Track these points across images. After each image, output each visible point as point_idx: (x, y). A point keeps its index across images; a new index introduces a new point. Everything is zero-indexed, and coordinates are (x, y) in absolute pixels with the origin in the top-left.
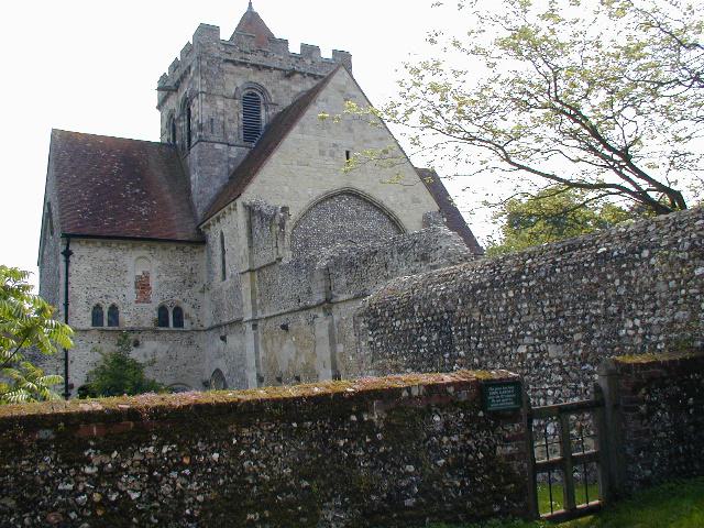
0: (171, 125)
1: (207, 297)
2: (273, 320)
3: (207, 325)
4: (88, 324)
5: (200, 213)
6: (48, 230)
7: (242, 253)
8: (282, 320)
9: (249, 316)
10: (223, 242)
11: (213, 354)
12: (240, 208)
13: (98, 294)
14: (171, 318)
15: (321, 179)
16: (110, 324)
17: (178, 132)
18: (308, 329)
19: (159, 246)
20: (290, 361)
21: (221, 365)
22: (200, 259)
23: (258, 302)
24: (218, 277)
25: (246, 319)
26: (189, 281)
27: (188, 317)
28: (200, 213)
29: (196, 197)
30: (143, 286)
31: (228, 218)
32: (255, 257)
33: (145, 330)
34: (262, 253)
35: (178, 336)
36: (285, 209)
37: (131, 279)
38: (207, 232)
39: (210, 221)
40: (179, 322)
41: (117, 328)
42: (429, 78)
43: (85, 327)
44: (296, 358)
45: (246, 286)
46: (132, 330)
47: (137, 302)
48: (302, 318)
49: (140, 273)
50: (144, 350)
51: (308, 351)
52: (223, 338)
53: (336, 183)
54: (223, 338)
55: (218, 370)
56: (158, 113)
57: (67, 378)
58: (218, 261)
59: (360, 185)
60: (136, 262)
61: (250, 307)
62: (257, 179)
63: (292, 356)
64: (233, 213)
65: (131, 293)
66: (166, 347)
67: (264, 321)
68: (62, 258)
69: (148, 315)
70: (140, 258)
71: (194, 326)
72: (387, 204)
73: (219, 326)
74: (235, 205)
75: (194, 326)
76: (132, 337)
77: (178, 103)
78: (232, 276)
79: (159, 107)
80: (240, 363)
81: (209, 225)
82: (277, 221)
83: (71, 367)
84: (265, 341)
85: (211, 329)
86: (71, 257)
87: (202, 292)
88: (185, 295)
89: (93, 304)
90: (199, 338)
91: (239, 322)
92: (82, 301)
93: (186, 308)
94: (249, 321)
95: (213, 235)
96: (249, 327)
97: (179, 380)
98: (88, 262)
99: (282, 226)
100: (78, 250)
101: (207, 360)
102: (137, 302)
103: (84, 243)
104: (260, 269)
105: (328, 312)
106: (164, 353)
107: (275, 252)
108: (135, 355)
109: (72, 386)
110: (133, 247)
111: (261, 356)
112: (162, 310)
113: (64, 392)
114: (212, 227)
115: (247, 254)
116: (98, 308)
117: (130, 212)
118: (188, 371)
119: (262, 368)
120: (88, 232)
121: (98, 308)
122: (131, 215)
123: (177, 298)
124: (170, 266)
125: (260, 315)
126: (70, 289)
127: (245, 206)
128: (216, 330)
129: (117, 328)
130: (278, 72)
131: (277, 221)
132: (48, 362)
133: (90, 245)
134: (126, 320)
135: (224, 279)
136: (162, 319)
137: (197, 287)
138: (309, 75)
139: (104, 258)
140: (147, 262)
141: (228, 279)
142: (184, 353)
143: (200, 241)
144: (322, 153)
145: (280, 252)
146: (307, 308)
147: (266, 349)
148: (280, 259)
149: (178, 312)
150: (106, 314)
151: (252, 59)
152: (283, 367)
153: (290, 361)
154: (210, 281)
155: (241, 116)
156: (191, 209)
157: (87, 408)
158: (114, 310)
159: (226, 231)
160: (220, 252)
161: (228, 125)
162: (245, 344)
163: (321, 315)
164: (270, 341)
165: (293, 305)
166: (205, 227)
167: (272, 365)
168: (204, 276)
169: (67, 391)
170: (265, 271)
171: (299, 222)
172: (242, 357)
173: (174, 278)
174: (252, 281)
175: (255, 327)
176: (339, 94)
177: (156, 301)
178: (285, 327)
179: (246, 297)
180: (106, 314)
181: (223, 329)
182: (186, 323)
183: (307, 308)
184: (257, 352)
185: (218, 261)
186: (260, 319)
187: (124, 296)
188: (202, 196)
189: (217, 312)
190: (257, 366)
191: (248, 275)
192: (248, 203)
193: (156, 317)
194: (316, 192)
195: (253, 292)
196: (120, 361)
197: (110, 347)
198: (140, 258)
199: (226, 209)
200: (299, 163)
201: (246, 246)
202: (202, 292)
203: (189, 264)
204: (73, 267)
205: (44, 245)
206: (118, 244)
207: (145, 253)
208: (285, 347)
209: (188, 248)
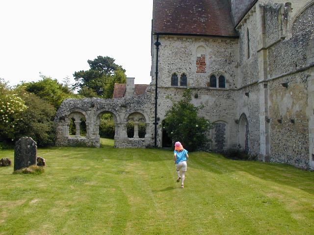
1: (239, 70)
2: (278, 81)
3: (239, 87)
4: (169, 84)
5: (236, 20)
7: (258, 38)
8: (284, 80)
9: (262, 79)
10: (248, 35)
11: (241, 104)
12: (258, 9)
13: (175, 67)
14: (217, 82)
16: (182, 84)
18: (302, 85)
19: (211, 40)
20: (288, 109)
21: (245, 110)
22: (236, 47)
23: (268, 69)
24: (245, 58)
25: (260, 81)
26: (229, 60)
27: (228, 82)
28: (236, 20)
29: (233, 12)
30: (201, 63)
31: (251, 18)
32: (267, 39)
33: (201, 88)
34: (272, 36)
35: (221, 93)
36: (288, 4)
37: (194, 59)
38: (240, 30)
40: (222, 85)
41: (185, 87)
43: (167, 86)
44: (292, 106)
45: (261, 59)
46: (194, 89)
47: (197, 72)
48: (298, 78)
49: (199, 55)
50: (201, 100)
51: (301, 102)
52: (247, 94)
54: (247, 94)
55: (244, 114)
57: (156, 114)
58: (245, 47)
60: (197, 49)
61: (263, 72)
63: (290, 106)
64: (254, 14)
65: (194, 67)
66: (214, 99)
67: (271, 82)
69: (204, 80)
70: (199, 46)
71: (231, 87)
73: (245, 87)
75: (231, 87)
76: (194, 92)
78: (253, 54)
80: (256, 110)
81: (241, 26)
82: (282, 11)
83: (158, 108)
84: (271, 95)
85: (240, 89)
86: (160, 47)
87: (237, 67)
88: (226, 69)
89: (172, 73)
90: (234, 95)
91: (256, 83)
92: (165, 71)
93: (227, 76)
95: (243, 32)
96: (262, 86)
97: (221, 119)
98: (169, 46)
99: (286, 15)
100: (163, 42)
101: (238, 108)
102: (197, 72)
103: (166, 38)
104: (269, 48)
106: (213, 103)
107: (280, 33)
108: (195, 103)
109: (159, 119)
110: (196, 40)
111: (269, 106)
112: (213, 77)
113: (154, 122)
114: (242, 27)
115: (262, 37)
116: (175, 75)
117: (195, 21)
118: (227, 114)
119: (269, 113)
120: (169, 31)
121: (175, 75)
122: (195, 22)
123: (221, 70)
125: (269, 78)
126: (159, 64)
127: (260, 6)
129: (185, 87)
131: (282, 11)
132: (146, 105)
134: (191, 82)
135: (249, 57)
136: (212, 83)
137: (234, 64)
139: (178, 47)
140: (204, 49)
142: (224, 103)
143: (236, 37)
145: (284, 33)
146: (302, 70)
147: (272, 101)
148: (283, 38)
149: (222, 79)
150: (179, 80)
152: (283, 113)
153: (288, 109)
154: (241, 59)
156: (231, 17)
157: (13, 165)
158: (184, 76)
159: (250, 27)
160: (247, 41)
162: (259, 97)
164: (275, 95)
165: (291, 69)
166: (238, 28)
167: (276, 112)
168: (237, 58)
170: (273, 48)
171: (298, 17)
172: (257, 107)
174: (265, 55)
175: (265, 86)
177: (209, 72)
178: (285, 85)
179: (261, 66)
180: (179, 80)
181: (247, 89)
182: (227, 85)
183: (302, 70)
184: (266, 103)
185: (245, 47)
186: (269, 81)
187: (191, 69)
188: (237, 10)
189: (245, 79)
190: (266, 111)
192: (263, 4)
193: (209, 81)
195: (265, 63)
196: (184, 106)
197: (179, 98)
201: (261, 33)
202: (237, 67)
203: (230, 50)
204: (161, 52)
206: (187, 39)
207: (202, 44)
208: (285, 99)
209: (228, 41)
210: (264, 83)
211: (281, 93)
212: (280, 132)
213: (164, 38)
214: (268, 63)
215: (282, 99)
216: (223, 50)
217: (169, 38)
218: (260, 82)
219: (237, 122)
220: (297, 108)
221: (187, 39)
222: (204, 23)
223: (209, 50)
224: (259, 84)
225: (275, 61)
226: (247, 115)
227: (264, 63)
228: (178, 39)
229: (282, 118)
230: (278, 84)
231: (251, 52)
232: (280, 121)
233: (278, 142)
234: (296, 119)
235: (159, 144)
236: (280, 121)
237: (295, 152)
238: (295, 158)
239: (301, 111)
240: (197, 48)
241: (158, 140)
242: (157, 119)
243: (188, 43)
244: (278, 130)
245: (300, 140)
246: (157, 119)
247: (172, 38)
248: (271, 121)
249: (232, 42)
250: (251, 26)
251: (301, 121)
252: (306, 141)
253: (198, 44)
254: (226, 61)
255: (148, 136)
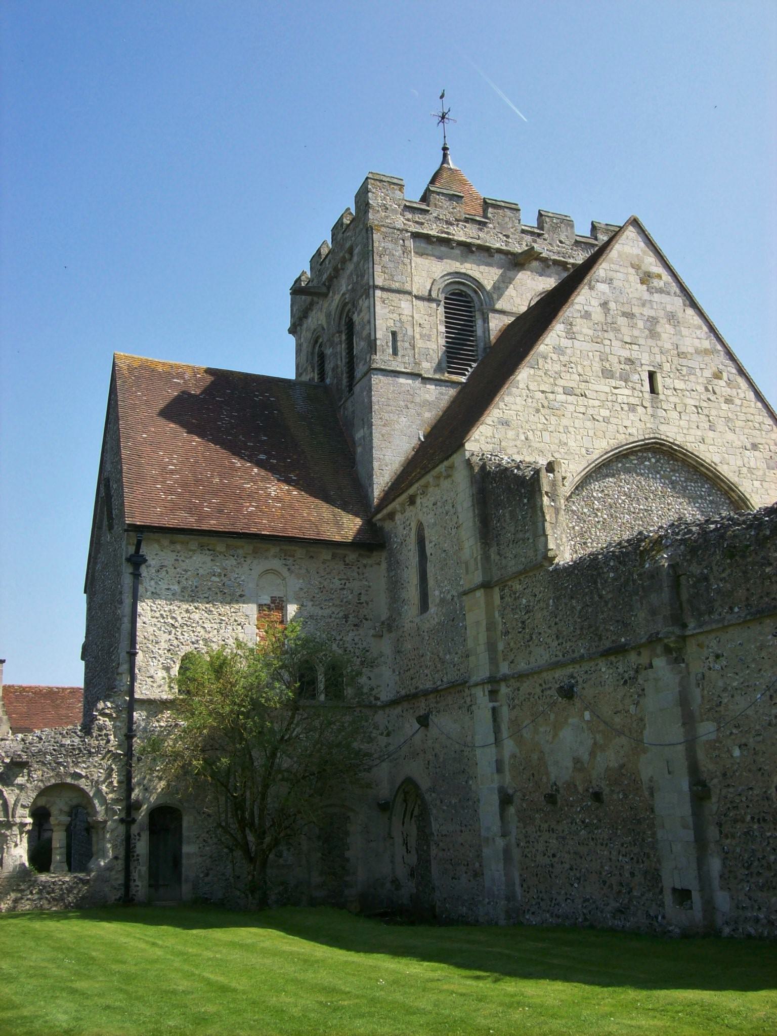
0: (313, 354)
6: (105, 523)
9: (484, 672)
15: (606, 420)
17: (329, 366)
20: (577, 761)
23: (501, 646)
25: (475, 679)
38: (388, 526)
39: (395, 505)
42: (345, 600)
44: (592, 754)
53: (634, 428)
54: (424, 721)
56: (292, 340)
59: (678, 431)
62: (493, 415)
68: (127, 569)
70: (267, 572)
72: (727, 471)
74: (451, 467)
77: (328, 315)
78: (443, 600)
79: (292, 331)
81: (426, 486)
85: (394, 703)
86: (143, 570)
91: (460, 686)
94: (482, 683)
96: (481, 696)
105: (676, 655)
110: (255, 551)
114: (398, 517)
124: (321, 589)
125: (504, 669)
128: (405, 705)
130: (503, 257)
133: (178, 547)
138: (556, 262)
139: (201, 571)
140: (279, 581)
141: (432, 609)
144: (607, 374)
146: (620, 650)
147: (517, 734)
150: (321, 678)
151: (460, 234)
152: (560, 769)
153: (577, 761)
155: (442, 329)
161: (419, 344)
163: (660, 662)
169: (128, 813)
173: (327, 612)
176: (632, 271)
185: (411, 576)
186: (505, 679)
191: (480, 594)
194: (602, 445)
198: (267, 572)
199: (429, 478)
200: (568, 392)
205: (95, 563)
207: (276, 564)
208: (567, 734)
210: (488, 687)
211: (552, 717)
212: (551, 830)
213: (158, 541)
214: (500, 627)
215: (555, 735)
216: (337, 583)
217: (173, 542)
218: (476, 685)
219: (385, 807)
220: (610, 758)
221: (228, 547)
222: (277, 499)
223: (295, 583)
224: (473, 691)
225: (523, 623)
226: (424, 783)
227: (488, 629)
228: (202, 546)
229: (557, 790)
230: (538, 690)
231: (435, 594)
232: (551, 799)
233: (547, 861)
234: (606, 791)
235: (140, 886)
236: (551, 799)
237: (611, 886)
238: (614, 905)
239: (622, 766)
240: (260, 576)
241: (135, 875)
242: (131, 807)
243: (231, 562)
244: (545, 826)
245: (623, 850)
246: (131, 807)
247: (182, 543)
248: (517, 800)
249: (365, 562)
250: (431, 515)
251: (626, 796)
252: (647, 850)
253: (259, 566)
254: (346, 617)
255: (107, 855)
